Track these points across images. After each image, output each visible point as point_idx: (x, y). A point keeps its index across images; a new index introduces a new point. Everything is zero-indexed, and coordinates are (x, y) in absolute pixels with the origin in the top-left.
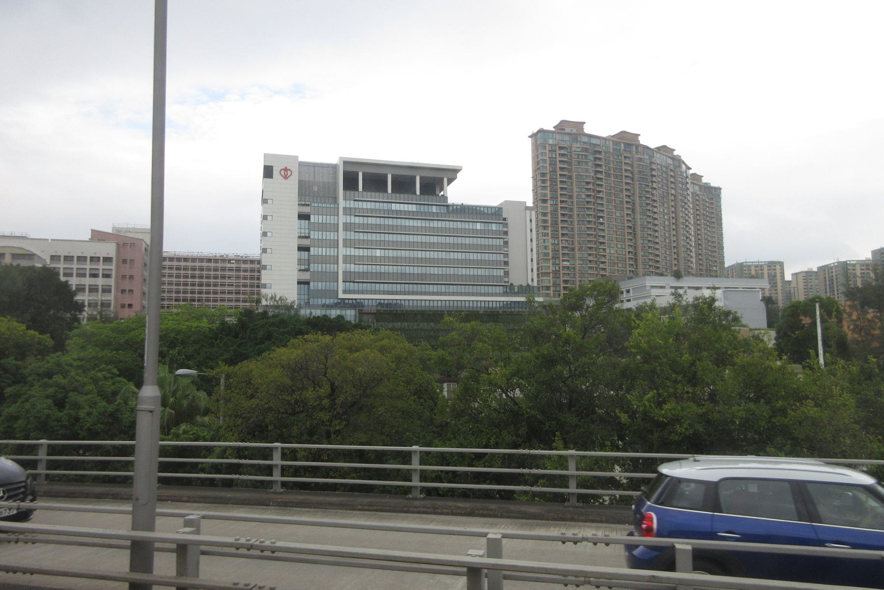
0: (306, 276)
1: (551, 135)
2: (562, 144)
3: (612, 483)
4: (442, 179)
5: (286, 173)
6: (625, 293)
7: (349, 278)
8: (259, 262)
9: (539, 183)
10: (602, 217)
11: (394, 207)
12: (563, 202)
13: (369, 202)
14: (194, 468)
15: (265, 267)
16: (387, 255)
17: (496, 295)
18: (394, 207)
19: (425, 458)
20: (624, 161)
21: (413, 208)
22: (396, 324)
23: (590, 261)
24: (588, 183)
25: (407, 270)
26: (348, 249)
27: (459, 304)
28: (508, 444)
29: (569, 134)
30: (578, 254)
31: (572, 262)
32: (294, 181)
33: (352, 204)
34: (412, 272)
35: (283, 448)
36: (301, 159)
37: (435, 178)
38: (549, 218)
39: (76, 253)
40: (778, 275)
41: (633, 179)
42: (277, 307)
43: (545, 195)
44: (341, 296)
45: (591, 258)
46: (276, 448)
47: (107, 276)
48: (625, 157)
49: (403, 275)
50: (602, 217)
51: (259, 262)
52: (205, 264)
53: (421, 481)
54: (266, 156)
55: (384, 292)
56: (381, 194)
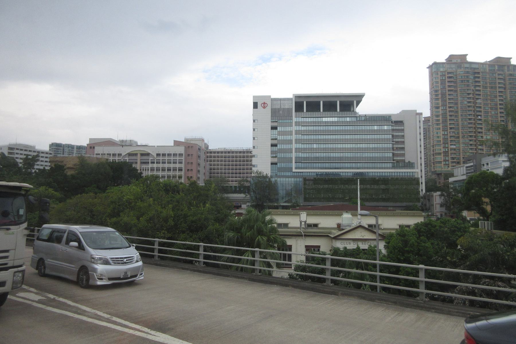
0: (275, 160)
3: (373, 278)
4: (353, 102)
5: (264, 105)
6: (485, 165)
7: (298, 160)
8: (251, 152)
9: (434, 97)
10: (480, 115)
11: (324, 119)
12: (451, 107)
13: (309, 118)
14: (171, 252)
15: (254, 156)
16: (320, 147)
17: (387, 168)
18: (324, 119)
20: (497, 77)
21: (336, 119)
22: (325, 186)
23: (471, 145)
24: (469, 94)
25: (332, 155)
26: (298, 145)
27: (411, 174)
28: (199, 238)
30: (461, 140)
31: (457, 146)
32: (268, 109)
33: (301, 120)
34: (371, 156)
35: (204, 246)
36: (272, 97)
37: (350, 102)
38: (440, 118)
39: (167, 152)
41: (505, 88)
42: (259, 177)
43: (438, 104)
44: (294, 170)
45: (471, 143)
46: (257, 251)
47: (181, 163)
48: (499, 74)
49: (329, 158)
50: (480, 115)
51: (251, 152)
52: (238, 154)
53: (331, 276)
54: (254, 97)
55: (319, 168)
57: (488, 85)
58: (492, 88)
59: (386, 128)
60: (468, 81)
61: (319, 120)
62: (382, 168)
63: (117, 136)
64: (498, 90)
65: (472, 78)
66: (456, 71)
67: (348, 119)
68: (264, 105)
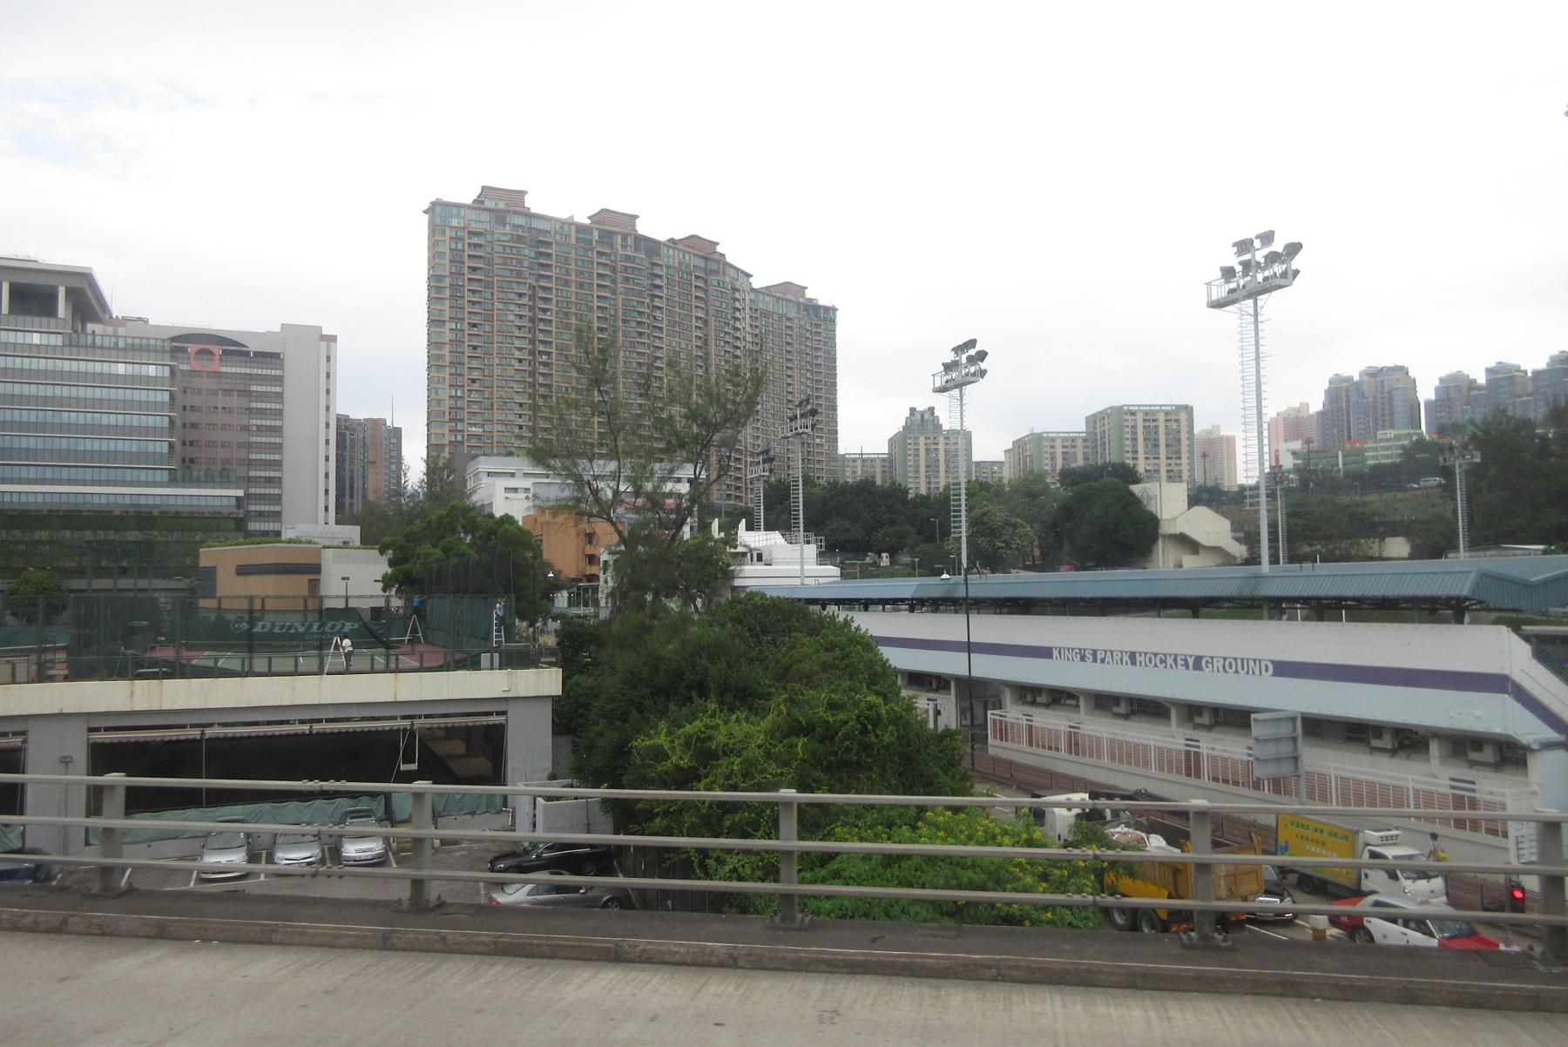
1: (455, 211)
2: (474, 227)
12: (475, 325)
17: (154, 484)
38: (446, 351)
40: (962, 453)
56: (45, 320)
57: (573, 277)
60: (520, 262)
62: (139, 484)
63: (1166, 621)
65: (533, 255)
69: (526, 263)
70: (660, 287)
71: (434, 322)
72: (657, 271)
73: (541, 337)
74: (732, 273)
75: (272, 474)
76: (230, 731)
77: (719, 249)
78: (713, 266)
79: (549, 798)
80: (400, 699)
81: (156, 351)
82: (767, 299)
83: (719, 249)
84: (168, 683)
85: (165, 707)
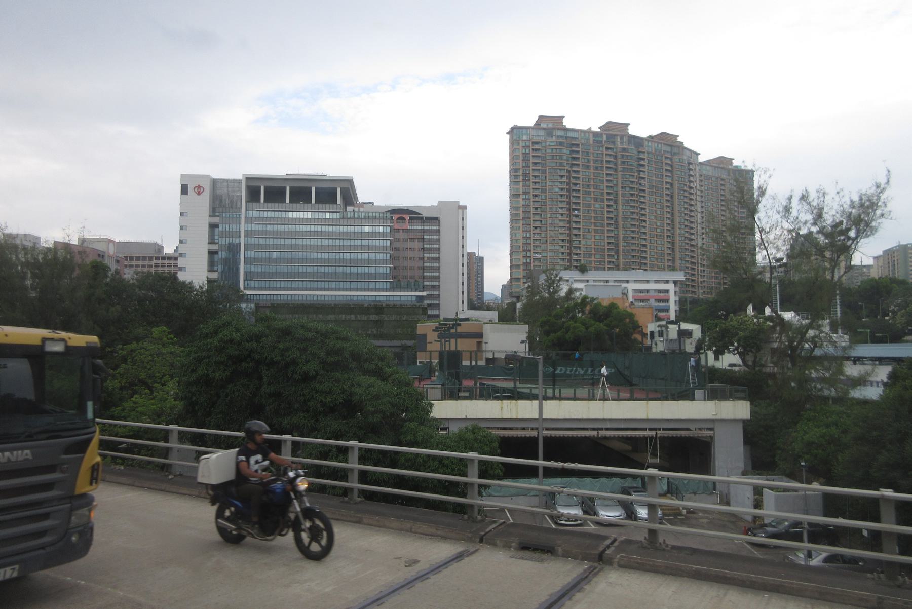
2: (535, 139)
5: (199, 190)
11: (292, 215)
12: (536, 196)
13: (267, 212)
17: (383, 290)
19: (365, 456)
20: (605, 152)
21: (308, 215)
29: (544, 129)
32: (206, 196)
33: (254, 214)
37: (306, 188)
43: (517, 189)
48: (607, 149)
57: (592, 164)
58: (597, 168)
59: (381, 229)
60: (561, 157)
61: (284, 215)
62: (376, 290)
64: (605, 172)
65: (568, 152)
66: (546, 142)
67: (328, 216)
68: (199, 190)
69: (565, 158)
70: (643, 165)
71: (514, 196)
72: (642, 156)
73: (574, 200)
74: (688, 153)
75: (435, 283)
76: (553, 433)
77: (679, 139)
78: (675, 150)
79: (771, 488)
80: (650, 417)
81: (379, 218)
82: (708, 168)
83: (679, 139)
84: (506, 403)
85: (520, 417)
